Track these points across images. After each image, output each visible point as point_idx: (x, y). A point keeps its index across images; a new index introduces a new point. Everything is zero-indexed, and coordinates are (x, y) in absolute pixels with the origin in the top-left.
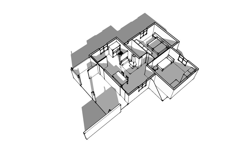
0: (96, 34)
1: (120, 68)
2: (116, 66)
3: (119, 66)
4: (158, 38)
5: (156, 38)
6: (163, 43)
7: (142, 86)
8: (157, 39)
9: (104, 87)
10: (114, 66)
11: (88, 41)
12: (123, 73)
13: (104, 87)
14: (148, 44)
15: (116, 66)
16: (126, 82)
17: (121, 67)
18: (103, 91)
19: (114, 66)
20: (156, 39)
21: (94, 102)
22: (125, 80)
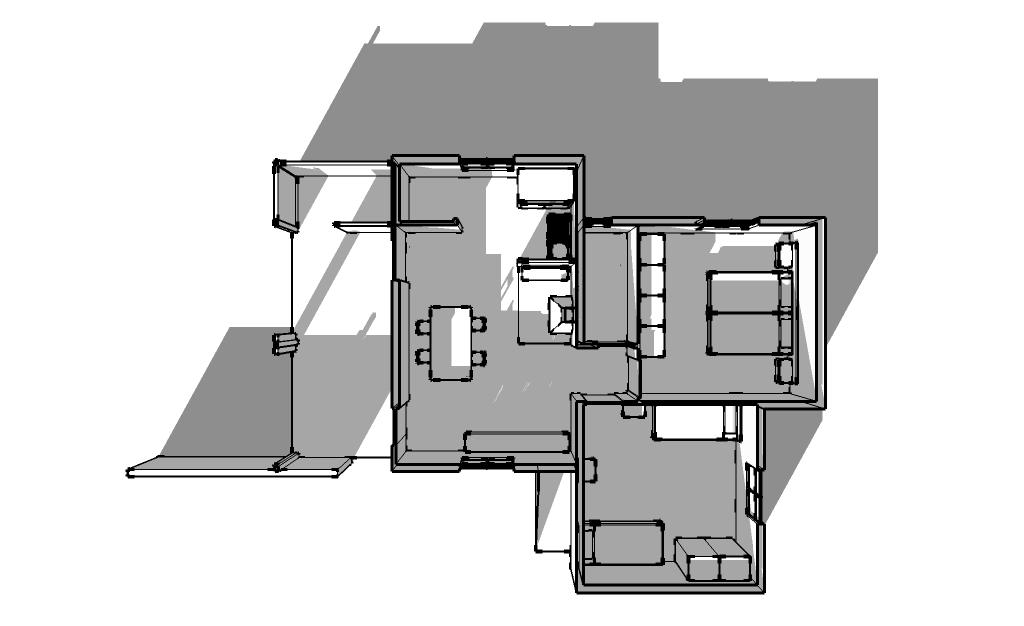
0: (557, 16)
1: (503, 278)
2: (498, 257)
3: (508, 265)
4: (786, 282)
5: (778, 268)
6: (780, 320)
7: (754, 492)
8: (780, 279)
9: (378, 30)
10: (488, 252)
11: (489, 31)
12: (479, 325)
13: (378, 30)
14: (716, 272)
15: (498, 257)
16: (526, 346)
17: (510, 278)
18: (352, 330)
19: (488, 252)
20: (774, 277)
21: (283, 343)
22: (650, 259)
